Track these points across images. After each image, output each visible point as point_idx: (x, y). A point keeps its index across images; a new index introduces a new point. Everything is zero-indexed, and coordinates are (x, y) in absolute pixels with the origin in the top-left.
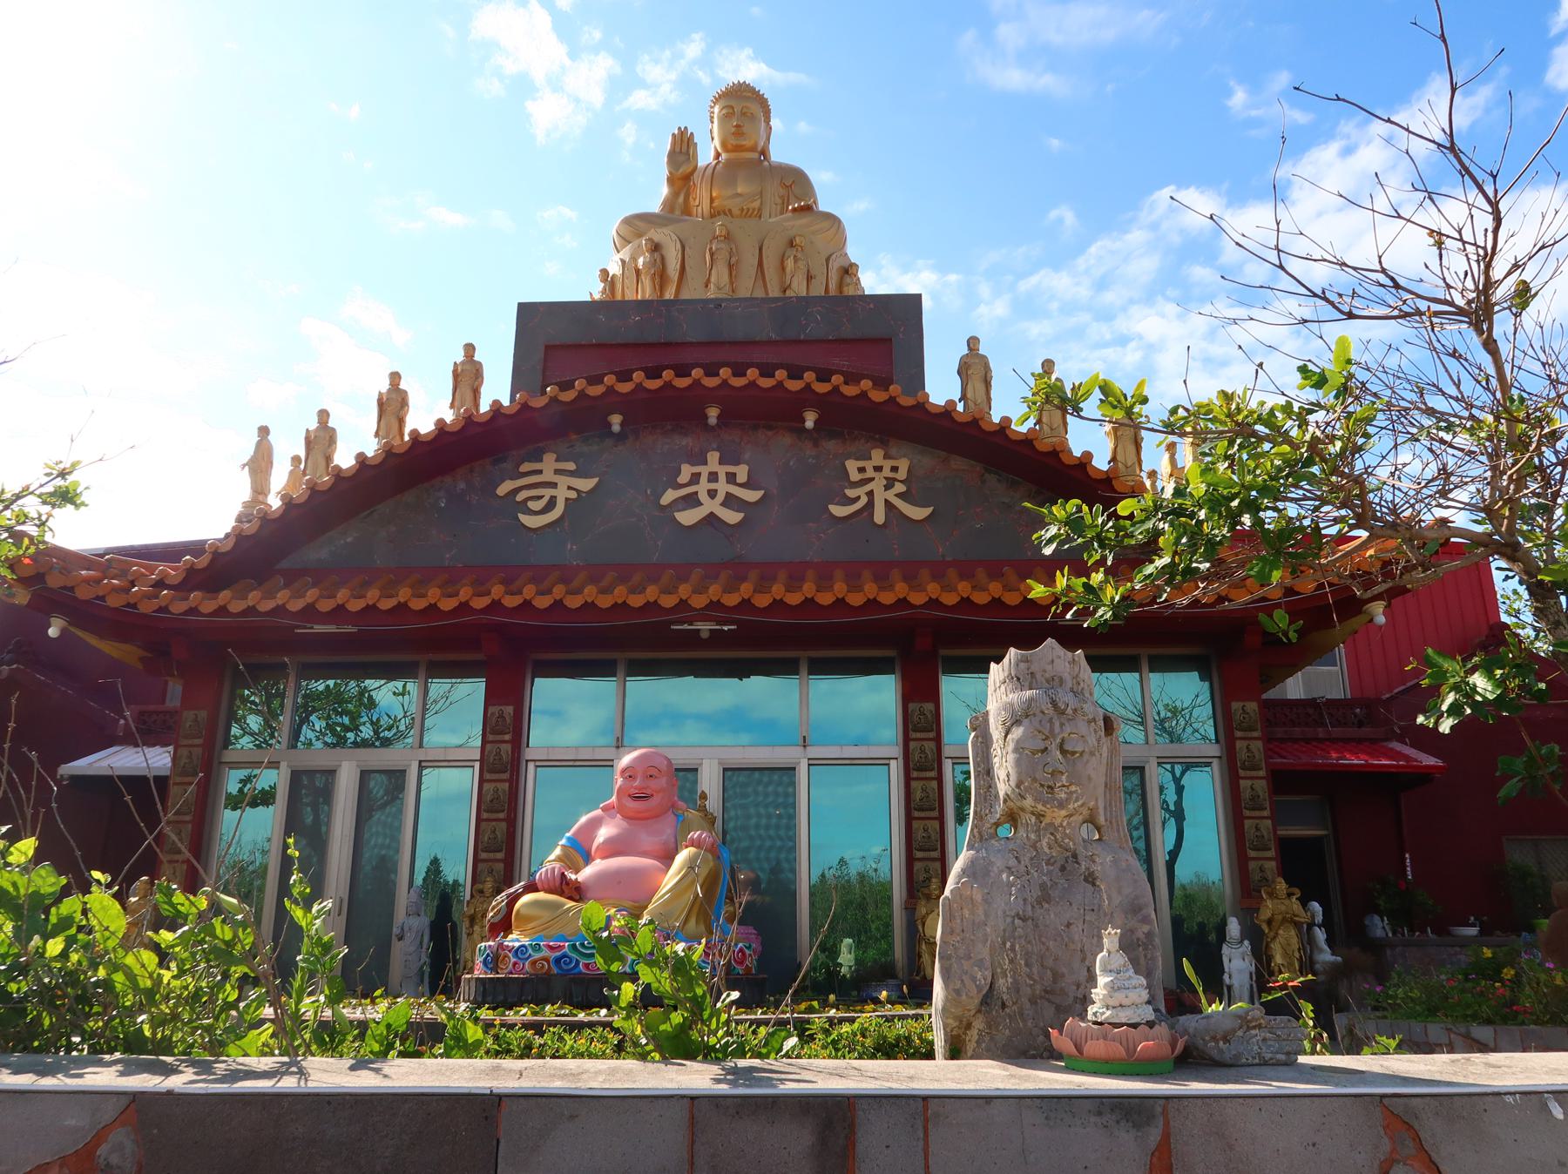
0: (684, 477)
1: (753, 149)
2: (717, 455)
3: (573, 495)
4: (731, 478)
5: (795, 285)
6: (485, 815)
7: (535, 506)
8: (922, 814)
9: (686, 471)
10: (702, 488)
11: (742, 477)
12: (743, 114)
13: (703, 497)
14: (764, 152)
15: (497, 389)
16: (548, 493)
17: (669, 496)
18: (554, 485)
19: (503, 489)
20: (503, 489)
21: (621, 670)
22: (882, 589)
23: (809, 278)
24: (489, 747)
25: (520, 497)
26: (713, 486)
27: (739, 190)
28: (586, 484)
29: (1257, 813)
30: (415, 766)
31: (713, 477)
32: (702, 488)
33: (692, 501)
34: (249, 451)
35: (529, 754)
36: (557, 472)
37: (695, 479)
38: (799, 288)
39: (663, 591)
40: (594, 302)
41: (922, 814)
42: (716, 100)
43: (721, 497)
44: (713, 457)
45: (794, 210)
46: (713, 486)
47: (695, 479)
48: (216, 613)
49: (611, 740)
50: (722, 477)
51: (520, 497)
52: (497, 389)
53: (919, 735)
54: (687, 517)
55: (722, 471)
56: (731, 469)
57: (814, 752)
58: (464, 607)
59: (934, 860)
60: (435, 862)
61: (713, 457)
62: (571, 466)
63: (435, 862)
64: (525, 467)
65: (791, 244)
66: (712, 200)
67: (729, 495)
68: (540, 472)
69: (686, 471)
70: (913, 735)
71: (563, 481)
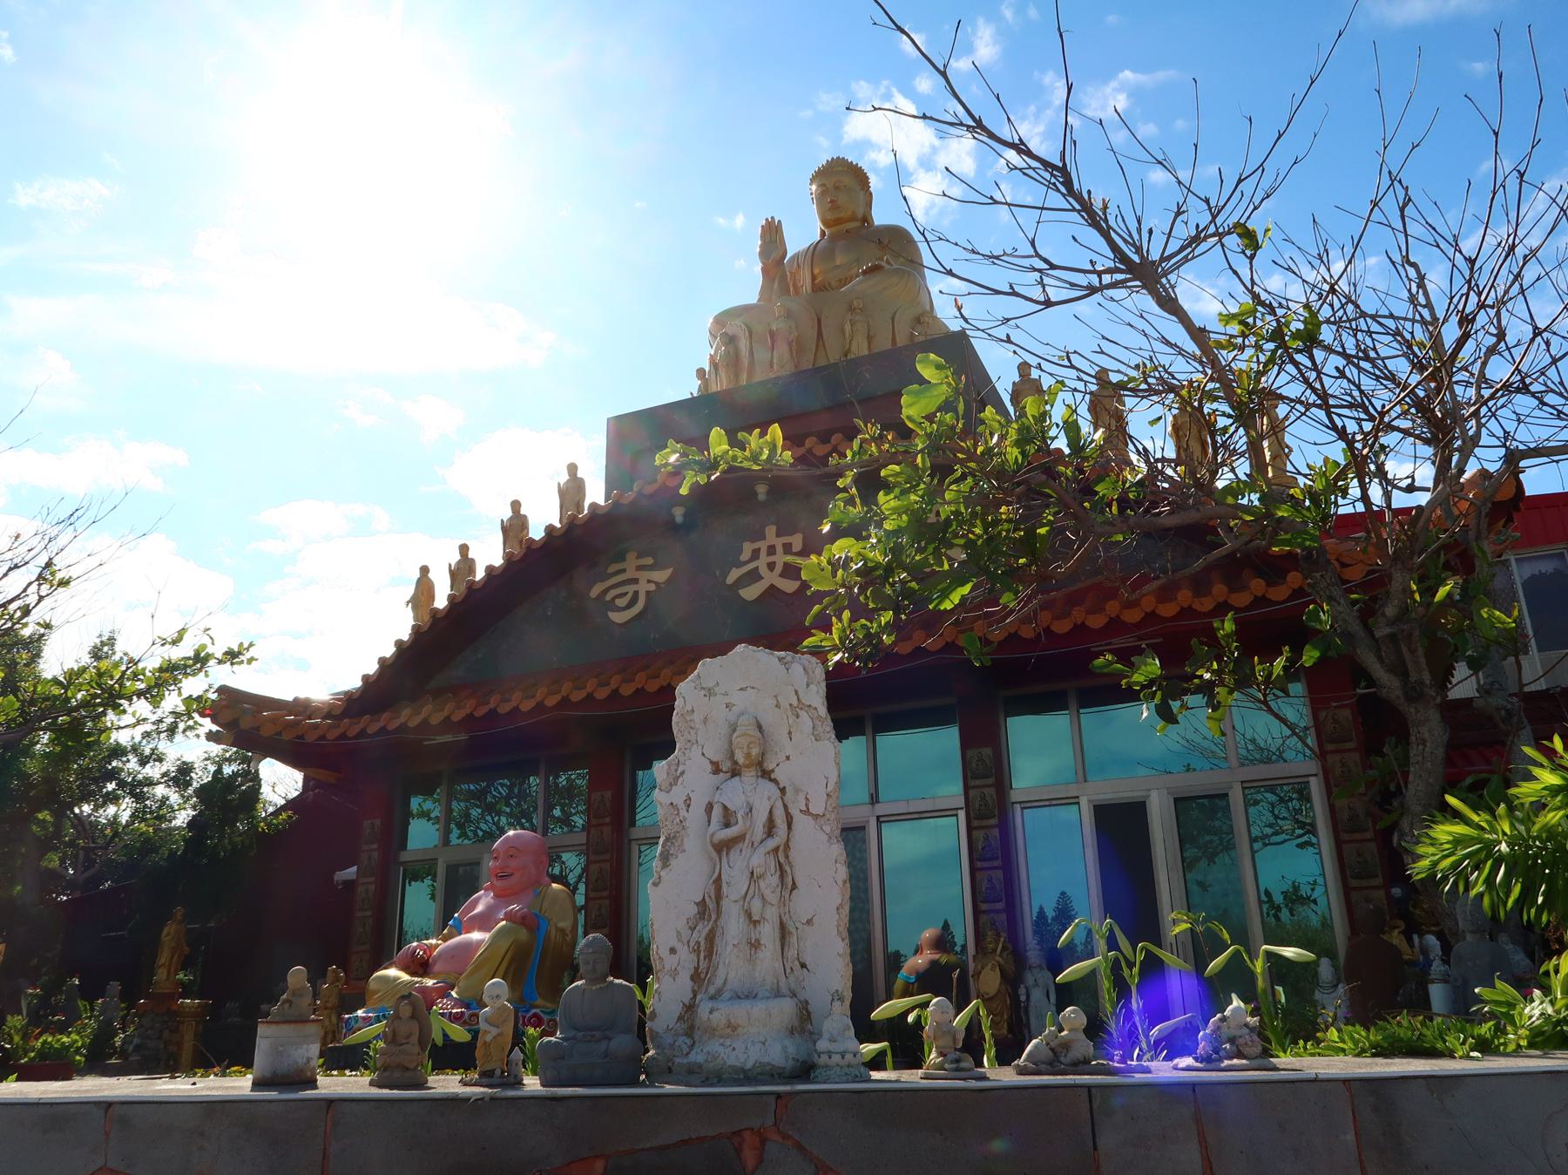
0: (745, 556)
1: (853, 218)
2: (774, 528)
3: (652, 587)
4: (787, 549)
5: (854, 348)
6: (592, 895)
7: (621, 602)
8: (986, 864)
9: (748, 548)
10: (761, 563)
11: (797, 546)
12: (837, 188)
13: (764, 571)
14: (866, 219)
15: (596, 494)
16: (631, 589)
17: (734, 575)
18: (635, 581)
19: (595, 592)
20: (595, 592)
21: (1073, 703)
22: (1232, 590)
23: (870, 339)
24: (972, 793)
25: (608, 597)
26: (771, 559)
27: (838, 262)
28: (661, 576)
29: (1357, 836)
30: (873, 822)
31: (771, 550)
32: (761, 563)
33: (754, 576)
34: (410, 591)
35: (1015, 796)
36: (639, 568)
37: (756, 554)
38: (860, 348)
39: (1089, 612)
40: (693, 399)
41: (986, 864)
42: (812, 181)
43: (779, 568)
44: (771, 531)
45: (865, 272)
46: (771, 559)
47: (756, 554)
48: (559, 705)
49: (867, 799)
50: (779, 549)
51: (608, 597)
52: (596, 494)
53: (978, 782)
54: (750, 593)
55: (779, 543)
56: (786, 539)
57: (881, 809)
58: (540, 707)
59: (998, 911)
60: (1041, 909)
61: (771, 531)
62: (649, 561)
63: (1041, 909)
64: (611, 569)
65: (851, 309)
66: (814, 278)
67: (786, 565)
68: (624, 571)
69: (748, 548)
70: (972, 783)
71: (644, 576)
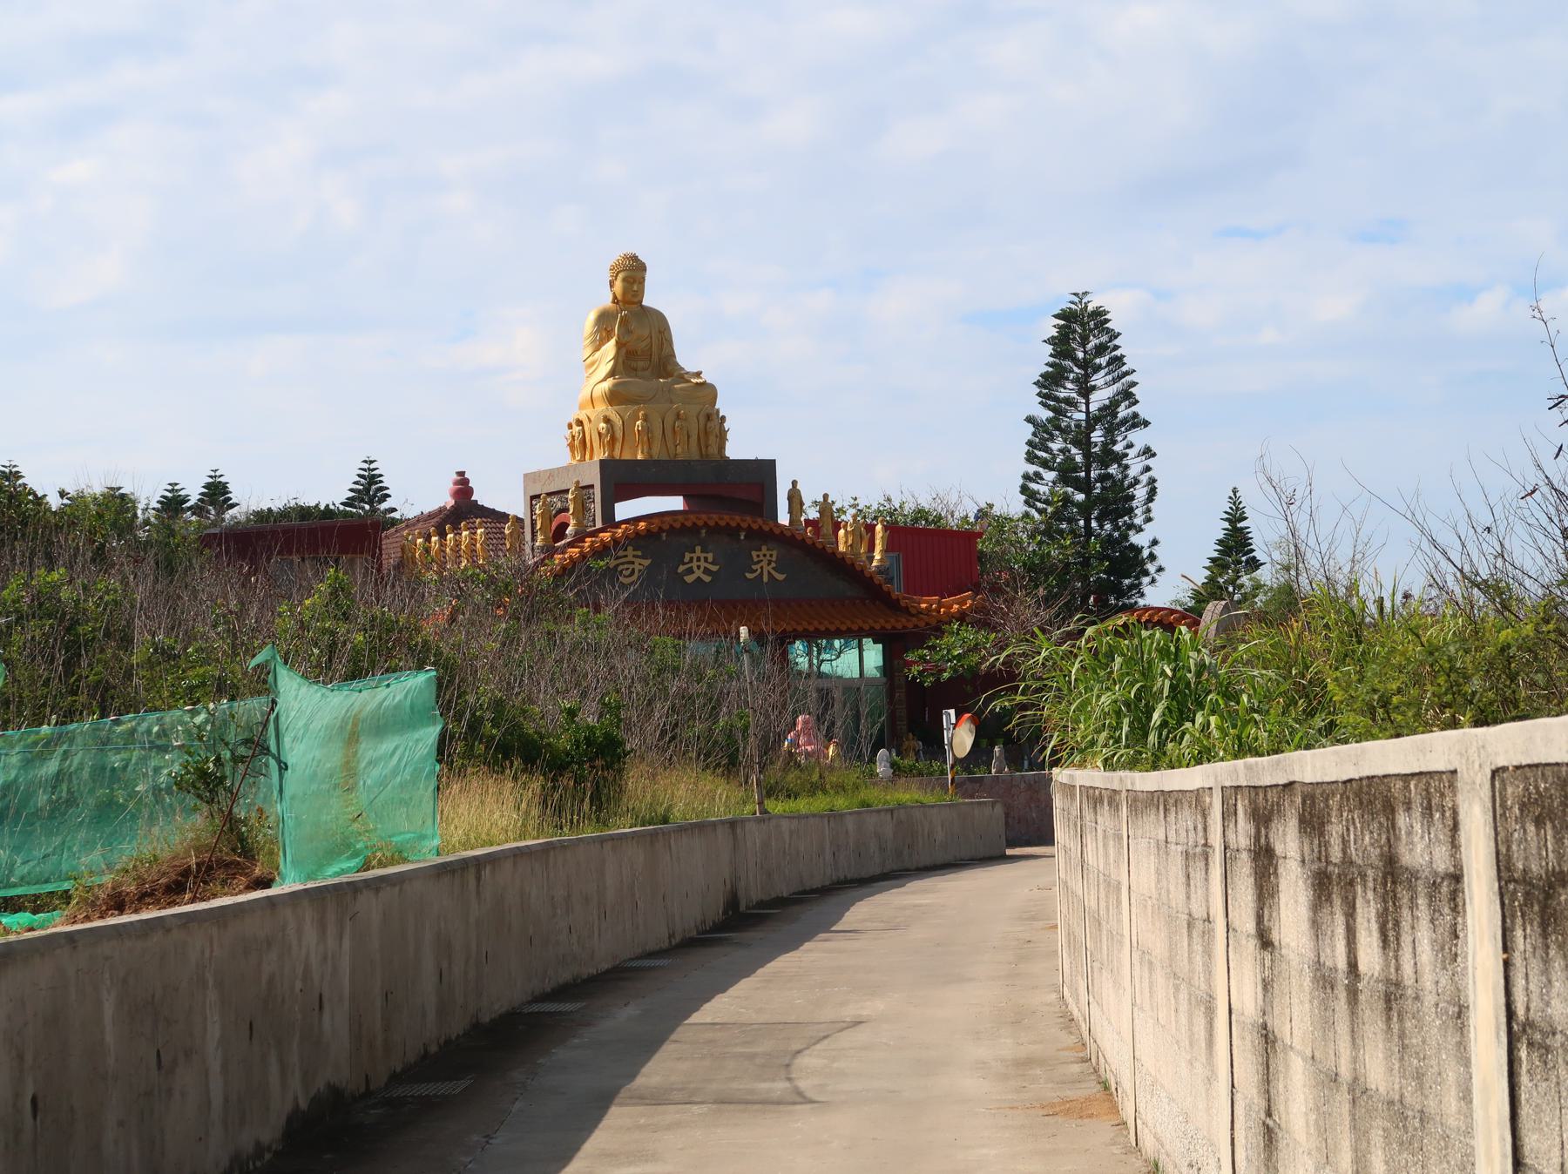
4: (706, 559)
32: (694, 565)
33: (690, 571)
37: (691, 560)
44: (698, 549)
47: (691, 560)
54: (689, 579)
61: (698, 549)
